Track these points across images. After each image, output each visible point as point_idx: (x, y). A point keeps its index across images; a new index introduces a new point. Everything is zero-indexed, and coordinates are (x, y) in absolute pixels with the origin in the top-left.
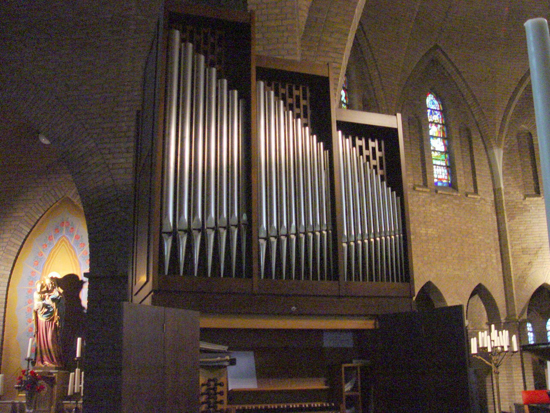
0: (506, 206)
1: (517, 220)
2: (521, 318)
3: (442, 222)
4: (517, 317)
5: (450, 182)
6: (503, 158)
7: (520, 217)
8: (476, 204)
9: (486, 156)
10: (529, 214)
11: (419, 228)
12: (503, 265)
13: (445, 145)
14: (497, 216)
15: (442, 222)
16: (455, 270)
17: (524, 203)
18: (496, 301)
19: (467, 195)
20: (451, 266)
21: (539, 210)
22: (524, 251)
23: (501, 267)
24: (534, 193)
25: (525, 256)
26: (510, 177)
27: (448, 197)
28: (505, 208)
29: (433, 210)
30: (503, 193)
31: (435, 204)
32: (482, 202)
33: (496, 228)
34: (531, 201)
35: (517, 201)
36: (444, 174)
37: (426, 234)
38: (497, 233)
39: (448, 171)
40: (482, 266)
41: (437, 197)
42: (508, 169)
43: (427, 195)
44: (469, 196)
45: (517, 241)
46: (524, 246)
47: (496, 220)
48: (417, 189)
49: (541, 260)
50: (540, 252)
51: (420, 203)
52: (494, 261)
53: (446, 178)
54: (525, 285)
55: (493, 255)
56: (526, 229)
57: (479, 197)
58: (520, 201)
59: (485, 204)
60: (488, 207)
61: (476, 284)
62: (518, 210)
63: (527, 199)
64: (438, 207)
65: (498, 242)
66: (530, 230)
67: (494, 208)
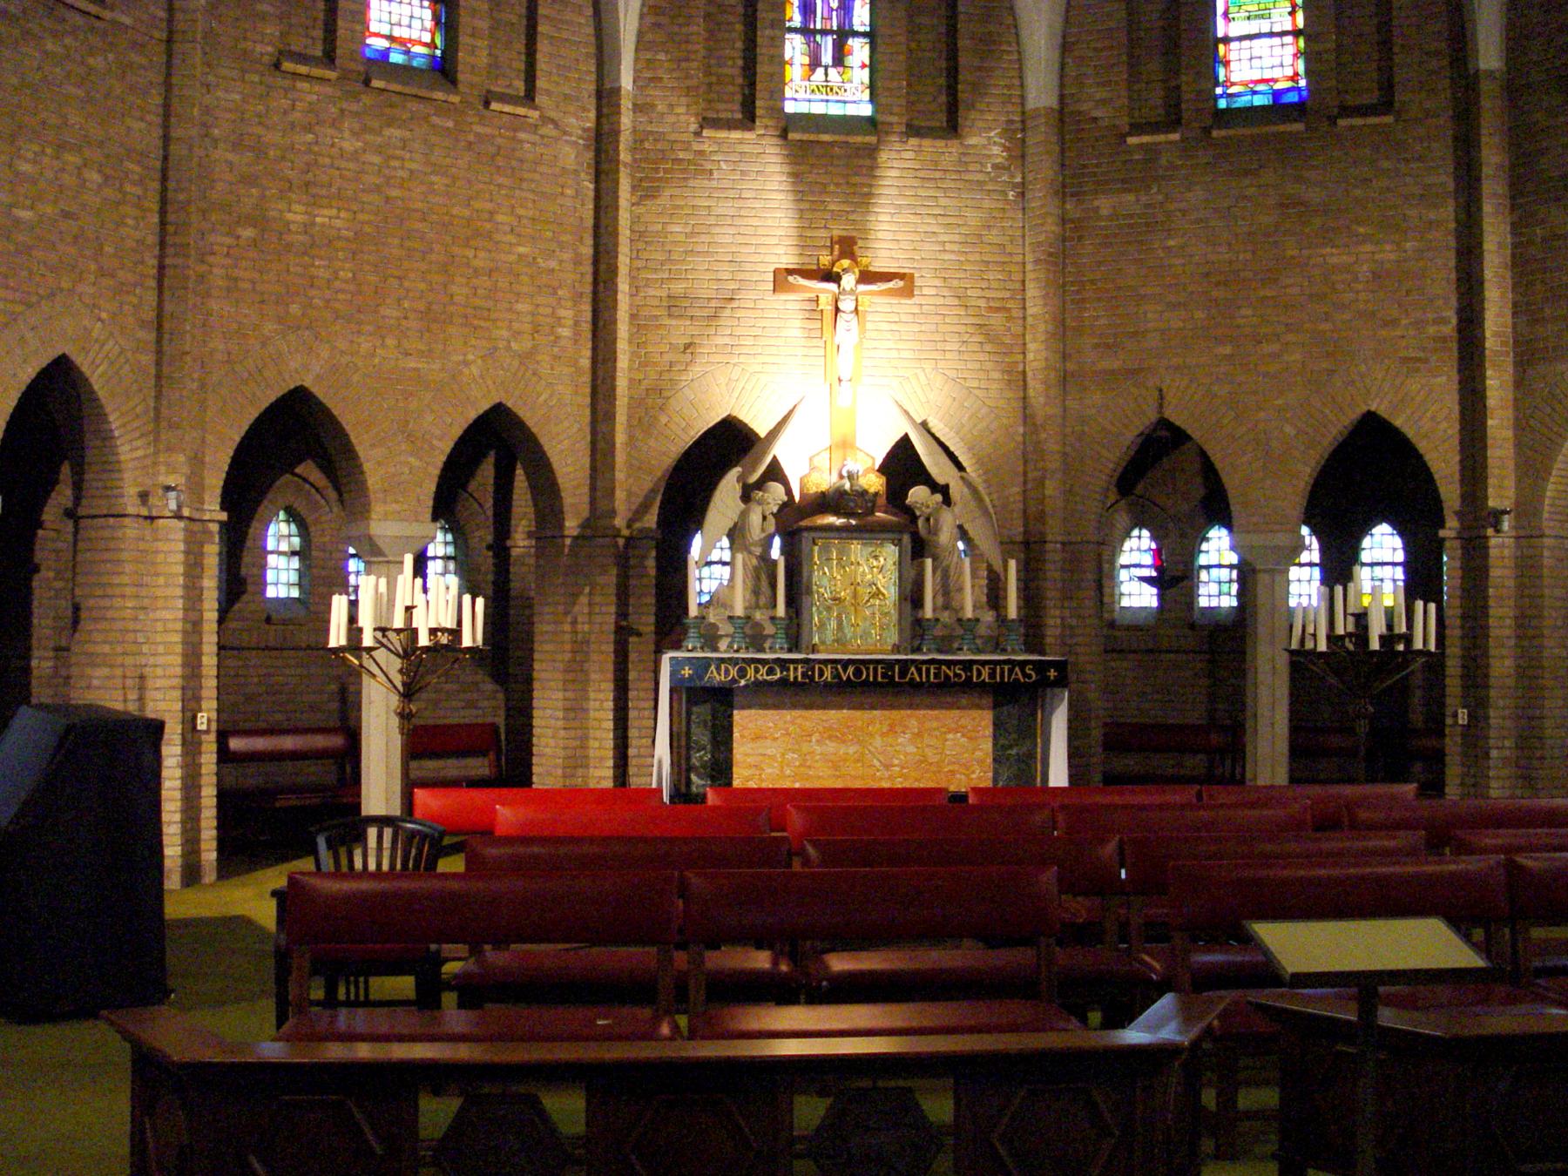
0: (633, 150)
1: (663, 201)
2: (638, 525)
3: (378, 189)
4: (619, 522)
5: (438, 53)
7: (676, 192)
8: (522, 135)
11: (282, 205)
12: (594, 349)
15: (378, 189)
16: (407, 354)
17: (696, 147)
18: (555, 465)
19: (487, 104)
20: (390, 342)
22: (674, 306)
23: (589, 353)
24: (739, 116)
25: (673, 322)
26: (661, 56)
27: (413, 105)
28: (625, 156)
29: (346, 145)
30: (626, 104)
31: (356, 126)
32: (549, 130)
33: (589, 222)
34: (719, 143)
35: (673, 137)
36: (416, 24)
37: (307, 228)
38: (589, 241)
39: (436, 19)
40: (514, 346)
41: (367, 100)
42: (658, 25)
43: (329, 90)
44: (495, 106)
46: (678, 288)
47: (591, 194)
48: (287, 66)
49: (727, 340)
50: (727, 312)
51: (296, 116)
52: (565, 332)
53: (427, 38)
54: (664, 419)
55: (567, 314)
57: (536, 114)
58: (684, 137)
59: (557, 139)
60: (567, 148)
61: (485, 406)
62: (664, 169)
63: (705, 133)
64: (368, 137)
65: (588, 269)
66: (703, 238)
67: (589, 156)
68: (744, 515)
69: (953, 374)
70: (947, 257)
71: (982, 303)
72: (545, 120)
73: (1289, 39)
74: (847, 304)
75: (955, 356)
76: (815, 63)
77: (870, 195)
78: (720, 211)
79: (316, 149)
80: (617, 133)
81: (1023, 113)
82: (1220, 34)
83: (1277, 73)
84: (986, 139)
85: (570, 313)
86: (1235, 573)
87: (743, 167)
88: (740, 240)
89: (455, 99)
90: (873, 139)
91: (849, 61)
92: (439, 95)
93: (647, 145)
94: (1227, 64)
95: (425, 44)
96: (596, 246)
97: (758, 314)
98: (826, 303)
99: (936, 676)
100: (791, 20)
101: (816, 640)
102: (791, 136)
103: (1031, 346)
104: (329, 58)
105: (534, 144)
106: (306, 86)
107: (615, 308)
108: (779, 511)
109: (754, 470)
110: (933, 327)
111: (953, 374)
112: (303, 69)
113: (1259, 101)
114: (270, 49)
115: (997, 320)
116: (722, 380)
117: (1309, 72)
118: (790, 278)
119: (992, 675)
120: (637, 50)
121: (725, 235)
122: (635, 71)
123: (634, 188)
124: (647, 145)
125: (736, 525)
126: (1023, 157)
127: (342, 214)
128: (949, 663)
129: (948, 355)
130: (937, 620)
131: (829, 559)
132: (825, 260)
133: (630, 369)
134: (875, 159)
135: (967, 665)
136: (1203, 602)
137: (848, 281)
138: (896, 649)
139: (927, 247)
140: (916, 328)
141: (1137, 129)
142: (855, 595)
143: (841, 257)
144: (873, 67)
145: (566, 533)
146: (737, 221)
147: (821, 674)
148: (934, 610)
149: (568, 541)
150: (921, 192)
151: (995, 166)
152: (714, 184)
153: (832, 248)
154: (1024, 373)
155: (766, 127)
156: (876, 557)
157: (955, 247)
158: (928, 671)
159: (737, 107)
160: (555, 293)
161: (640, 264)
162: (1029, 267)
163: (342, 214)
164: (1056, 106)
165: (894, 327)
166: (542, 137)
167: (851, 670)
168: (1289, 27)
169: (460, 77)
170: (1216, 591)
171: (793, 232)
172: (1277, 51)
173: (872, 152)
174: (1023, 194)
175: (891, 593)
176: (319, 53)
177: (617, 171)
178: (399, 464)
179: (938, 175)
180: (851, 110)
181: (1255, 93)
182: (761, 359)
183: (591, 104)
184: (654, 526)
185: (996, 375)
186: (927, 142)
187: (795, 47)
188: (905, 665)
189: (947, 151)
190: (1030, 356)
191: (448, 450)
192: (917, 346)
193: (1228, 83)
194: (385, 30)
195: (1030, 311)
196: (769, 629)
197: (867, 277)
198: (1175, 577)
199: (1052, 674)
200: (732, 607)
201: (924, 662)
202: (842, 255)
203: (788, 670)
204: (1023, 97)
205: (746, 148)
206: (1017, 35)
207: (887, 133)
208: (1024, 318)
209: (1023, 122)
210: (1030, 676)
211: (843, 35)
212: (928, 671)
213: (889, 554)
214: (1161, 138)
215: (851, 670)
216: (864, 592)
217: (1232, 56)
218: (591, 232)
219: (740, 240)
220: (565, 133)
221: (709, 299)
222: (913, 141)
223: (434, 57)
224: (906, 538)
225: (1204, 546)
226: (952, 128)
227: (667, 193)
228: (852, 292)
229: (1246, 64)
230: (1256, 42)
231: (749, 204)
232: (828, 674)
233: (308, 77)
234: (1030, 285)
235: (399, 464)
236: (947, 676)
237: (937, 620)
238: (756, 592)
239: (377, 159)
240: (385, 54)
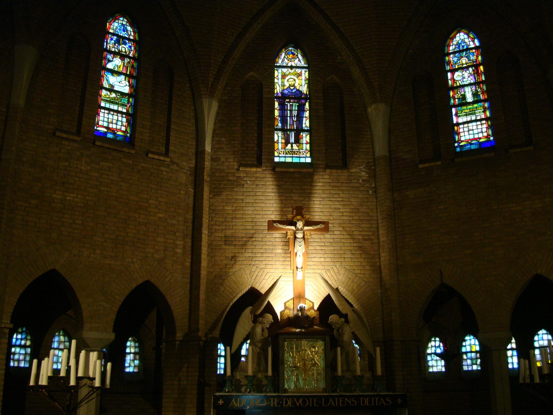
0: (210, 176)
1: (223, 197)
2: (210, 336)
5: (128, 135)
6: (218, 113)
7: (229, 193)
8: (163, 168)
9: (193, 108)
10: (241, 190)
13: (131, 86)
14: (195, 189)
17: (237, 175)
19: (147, 155)
20: (98, 251)
21: (257, 185)
22: (228, 240)
23: (190, 260)
24: (256, 163)
26: (223, 139)
29: (83, 168)
30: (207, 158)
32: (175, 167)
40: (155, 255)
44: (150, 155)
45: (219, 226)
46: (229, 233)
47: (192, 194)
48: (58, 134)
49: (250, 255)
50: (250, 243)
54: (222, 289)
56: (236, 210)
57: (168, 160)
61: (140, 281)
62: (224, 184)
65: (190, 225)
66: (241, 212)
67: (192, 178)
68: (253, 329)
69: (348, 268)
70: (344, 218)
71: (360, 237)
72: (172, 162)
73: (484, 122)
74: (300, 235)
75: (349, 260)
76: (287, 142)
77: (311, 193)
78: (247, 201)
79: (69, 168)
80: (203, 168)
81: (374, 159)
82: (455, 122)
83: (480, 135)
84: (359, 171)
85: (181, 243)
86: (478, 355)
87: (257, 183)
88: (256, 212)
89: (133, 152)
90: (311, 170)
91: (301, 141)
92: (125, 150)
93: (216, 174)
94: (458, 134)
95: (123, 132)
96: (194, 214)
97: (264, 243)
98: (290, 236)
99: (343, 403)
100: (277, 125)
101: (286, 386)
102: (277, 170)
103: (382, 255)
104: (78, 133)
105: (168, 172)
106: (66, 143)
107: (201, 240)
108: (270, 327)
109: (259, 308)
110: (339, 248)
111: (348, 268)
112: (64, 135)
113: (473, 147)
114: (52, 127)
115: (367, 244)
116: (248, 272)
117: (493, 135)
118: (275, 224)
119: (370, 402)
120: (213, 137)
121: (249, 211)
122: (212, 145)
123: (211, 192)
124: (216, 174)
125: (250, 333)
126: (375, 176)
127: (79, 196)
128: (348, 397)
129: (346, 260)
130: (344, 377)
131: (292, 348)
132: (290, 216)
133: (208, 267)
134: (313, 178)
135: (358, 398)
136: (465, 368)
137: (300, 224)
138: (324, 390)
139: (335, 214)
140: (332, 248)
141: (421, 162)
142: (304, 365)
143: (297, 215)
144: (311, 143)
145: (177, 339)
146: (255, 205)
147: (286, 403)
148: (342, 372)
149: (178, 343)
150: (332, 192)
151: (363, 181)
152: (245, 190)
153: (293, 211)
154: (380, 266)
155: (266, 167)
156: (314, 347)
157: (348, 214)
158: (339, 401)
159: (255, 159)
160: (175, 234)
161: (213, 223)
162: (380, 221)
163: (79, 196)
164: (387, 154)
165: (323, 248)
166: (172, 169)
167: (301, 400)
168: (483, 117)
169: (136, 143)
170: (471, 364)
171: (277, 209)
172: (480, 127)
173: (311, 176)
174: (375, 192)
175: (321, 363)
176: (75, 131)
177: (203, 184)
178: (100, 308)
179: (339, 184)
180: (303, 160)
181: (471, 144)
182: (264, 263)
183: (194, 157)
184: (218, 336)
185: (367, 268)
186: (334, 171)
187: (278, 137)
188: (327, 398)
189: (343, 175)
190: (382, 259)
191: (122, 300)
192: (332, 256)
193: (460, 141)
194: (106, 124)
195: (381, 240)
196: (265, 382)
197: (308, 223)
198: (452, 355)
199: (399, 401)
200: (247, 371)
201: (336, 396)
202: (297, 214)
203: (270, 401)
204: (374, 152)
205: (258, 175)
206: (370, 128)
207: (317, 168)
208: (379, 243)
209: (374, 162)
210: (389, 402)
211: (299, 131)
212: (339, 401)
213: (319, 346)
214: (433, 164)
215: (301, 400)
216: (309, 363)
217: (461, 130)
218: (192, 209)
219: (256, 212)
220: (181, 168)
221: (242, 237)
222: (328, 171)
223: (127, 136)
224: (328, 337)
225: (464, 344)
226: (344, 165)
227: (225, 194)
228: (302, 229)
229: (466, 133)
230: (470, 124)
231: (259, 198)
232: (289, 403)
233: (67, 139)
234: (380, 229)
235: (100, 308)
236: (348, 403)
237: (344, 377)
238: (259, 364)
239: (96, 174)
240: (106, 133)
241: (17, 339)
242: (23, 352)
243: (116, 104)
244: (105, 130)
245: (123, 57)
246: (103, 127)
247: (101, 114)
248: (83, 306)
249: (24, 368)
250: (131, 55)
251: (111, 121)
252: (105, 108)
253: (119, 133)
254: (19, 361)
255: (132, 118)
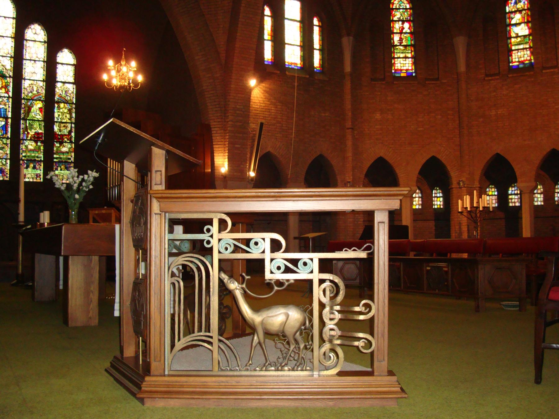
13: (529, 28)
112: (490, 78)
136: (8, 179)
194: (517, 60)
240: (518, 65)
241: (512, 191)
242: (516, 197)
243: (522, 44)
244: (517, 64)
245: (520, 11)
246: (515, 62)
247: (513, 55)
248: (516, 170)
249: (518, 206)
250: (526, 8)
251: (521, 55)
252: (515, 50)
253: (527, 62)
254: (515, 202)
255: (533, 50)
